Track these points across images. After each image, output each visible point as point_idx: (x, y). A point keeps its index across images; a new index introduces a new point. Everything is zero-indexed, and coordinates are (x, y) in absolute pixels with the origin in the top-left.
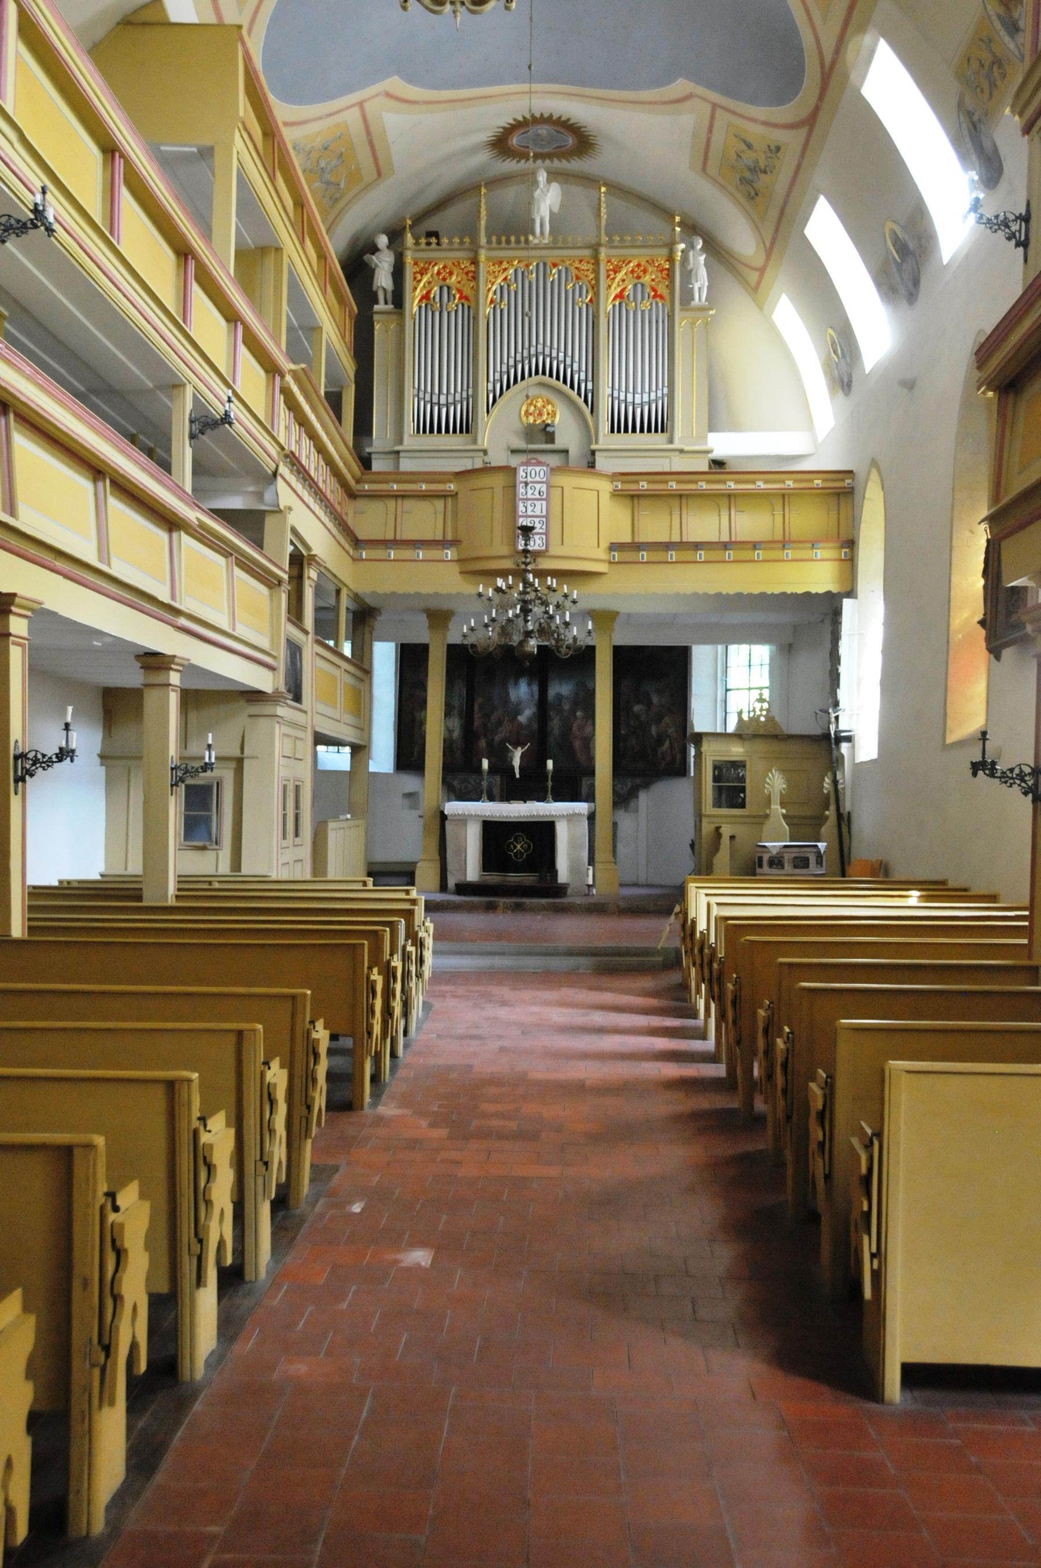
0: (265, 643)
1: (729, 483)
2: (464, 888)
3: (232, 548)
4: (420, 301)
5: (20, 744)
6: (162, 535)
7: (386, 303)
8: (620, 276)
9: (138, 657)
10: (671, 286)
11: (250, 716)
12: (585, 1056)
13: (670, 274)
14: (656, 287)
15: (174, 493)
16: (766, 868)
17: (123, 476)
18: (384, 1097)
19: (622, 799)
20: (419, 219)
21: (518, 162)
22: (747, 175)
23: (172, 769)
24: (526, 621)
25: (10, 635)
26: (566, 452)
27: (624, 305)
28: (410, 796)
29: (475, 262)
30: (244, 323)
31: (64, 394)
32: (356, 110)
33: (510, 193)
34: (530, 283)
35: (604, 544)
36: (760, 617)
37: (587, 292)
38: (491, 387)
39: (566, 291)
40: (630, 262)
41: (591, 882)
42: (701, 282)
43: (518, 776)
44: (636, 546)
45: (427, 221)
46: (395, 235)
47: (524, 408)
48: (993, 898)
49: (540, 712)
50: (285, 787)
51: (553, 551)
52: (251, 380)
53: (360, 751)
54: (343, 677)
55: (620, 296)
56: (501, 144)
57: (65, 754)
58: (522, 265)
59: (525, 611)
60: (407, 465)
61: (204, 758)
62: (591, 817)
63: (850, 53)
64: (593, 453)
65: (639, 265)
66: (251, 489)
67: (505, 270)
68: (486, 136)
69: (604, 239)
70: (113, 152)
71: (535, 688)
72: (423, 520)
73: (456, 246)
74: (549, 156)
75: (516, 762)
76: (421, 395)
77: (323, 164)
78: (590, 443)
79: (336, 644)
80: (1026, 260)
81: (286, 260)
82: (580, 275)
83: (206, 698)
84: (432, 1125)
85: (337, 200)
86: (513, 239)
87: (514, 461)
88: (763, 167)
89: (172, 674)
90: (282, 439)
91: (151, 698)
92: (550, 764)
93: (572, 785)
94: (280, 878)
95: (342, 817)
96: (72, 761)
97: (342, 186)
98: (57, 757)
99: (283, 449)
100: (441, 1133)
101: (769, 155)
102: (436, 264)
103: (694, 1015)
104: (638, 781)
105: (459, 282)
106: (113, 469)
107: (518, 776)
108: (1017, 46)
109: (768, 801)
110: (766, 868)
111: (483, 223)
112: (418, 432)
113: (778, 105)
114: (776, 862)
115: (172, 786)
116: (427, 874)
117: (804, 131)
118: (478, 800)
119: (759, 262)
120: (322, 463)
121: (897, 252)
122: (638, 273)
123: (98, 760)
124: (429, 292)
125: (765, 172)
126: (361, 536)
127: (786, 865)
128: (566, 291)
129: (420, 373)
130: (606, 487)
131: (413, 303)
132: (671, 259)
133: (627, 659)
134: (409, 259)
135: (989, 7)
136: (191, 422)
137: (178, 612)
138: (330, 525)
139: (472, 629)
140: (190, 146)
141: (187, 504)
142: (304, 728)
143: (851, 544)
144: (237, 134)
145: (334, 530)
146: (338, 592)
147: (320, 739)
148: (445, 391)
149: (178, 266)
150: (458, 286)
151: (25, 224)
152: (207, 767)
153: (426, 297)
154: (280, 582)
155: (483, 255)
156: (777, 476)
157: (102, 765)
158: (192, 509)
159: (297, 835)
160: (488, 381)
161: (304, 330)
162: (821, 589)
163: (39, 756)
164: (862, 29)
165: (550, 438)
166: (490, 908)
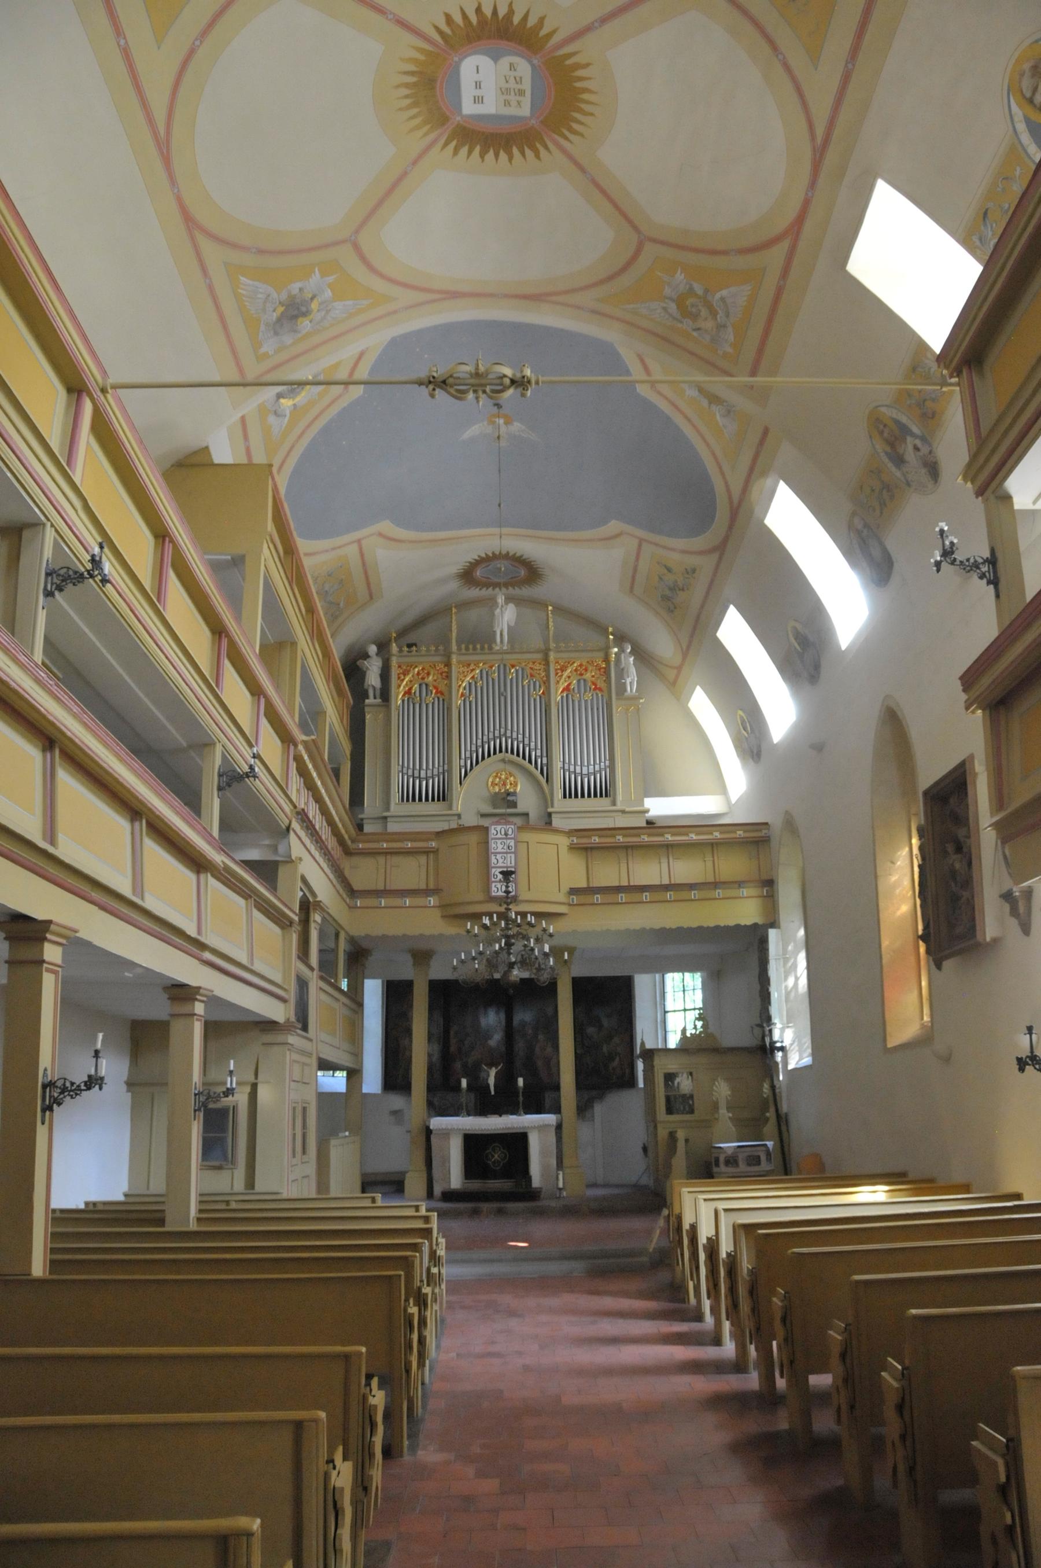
0: (278, 978)
1: (667, 836)
2: (449, 1196)
3: (251, 891)
4: (404, 695)
5: (49, 1072)
6: (190, 876)
8: (566, 674)
9: (166, 989)
10: (608, 680)
11: (264, 1044)
12: (609, 1372)
13: (607, 672)
15: (203, 838)
16: (723, 1168)
17: (158, 817)
18: (421, 1437)
19: (583, 1109)
20: (402, 633)
23: (195, 1095)
24: (509, 954)
25: (44, 961)
26: (527, 815)
28: (396, 1113)
29: (448, 664)
30: (266, 697)
31: (108, 735)
32: (355, 546)
33: (474, 615)
35: (565, 888)
36: (688, 949)
38: (463, 763)
39: (523, 687)
41: (561, 1185)
42: (631, 680)
43: (493, 1093)
44: (590, 890)
45: (409, 633)
46: (383, 647)
47: (491, 780)
48: (966, 1188)
49: (504, 1038)
50: (294, 1108)
52: (269, 745)
53: (354, 1074)
54: (340, 1008)
55: (567, 689)
56: (467, 576)
57: (93, 1082)
58: (486, 666)
59: (509, 945)
60: (393, 827)
61: (226, 1083)
62: (559, 1127)
63: (755, 493)
64: (550, 815)
65: (581, 665)
66: (267, 842)
67: (472, 670)
68: (455, 569)
69: (552, 645)
70: (164, 537)
71: (502, 1016)
72: (409, 873)
73: (433, 652)
74: (506, 585)
75: (492, 1081)
76: (405, 771)
77: (326, 588)
78: (547, 807)
79: (336, 981)
80: (998, 596)
81: (299, 653)
82: (534, 673)
83: (229, 1029)
84: (481, 1474)
85: (336, 617)
86: (478, 646)
87: (485, 822)
88: (681, 586)
89: (197, 1004)
90: (294, 799)
91: (177, 1028)
92: (521, 1082)
93: (537, 1100)
94: (290, 1196)
95: (341, 1135)
96: (101, 1089)
97: (342, 605)
98: (86, 1085)
99: (295, 807)
100: (491, 1485)
103: (699, 1318)
104: (594, 1093)
106: (150, 810)
107: (493, 1093)
108: (904, 475)
109: (715, 1107)
110: (723, 1168)
111: (454, 634)
113: (696, 536)
114: (732, 1161)
115: (195, 1111)
116: (415, 1184)
117: (715, 557)
118: (457, 1115)
119: (677, 660)
120: (325, 823)
121: (799, 644)
122: (580, 672)
123: (124, 1087)
124: (410, 689)
125: (683, 590)
126: (356, 886)
127: (740, 1163)
128: (523, 687)
129: (405, 754)
130: (564, 842)
131: (398, 697)
132: (607, 660)
133: (583, 987)
134: (394, 662)
135: (877, 447)
136: (220, 775)
137: (203, 947)
138: (331, 876)
139: (463, 962)
140: (226, 555)
141: (214, 848)
142: (309, 1055)
143: (769, 883)
144: (265, 546)
145: (334, 881)
146: (337, 935)
147: (325, 1065)
148: (424, 767)
149: (213, 643)
151: (82, 574)
152: (229, 1092)
153: (408, 692)
154: (292, 923)
155: (454, 659)
156: (705, 829)
157: (128, 1091)
158: (219, 853)
159: (304, 1152)
161: (312, 716)
162: (747, 921)
163: (68, 1084)
164: (764, 474)
165: (514, 805)
166: (475, 1213)
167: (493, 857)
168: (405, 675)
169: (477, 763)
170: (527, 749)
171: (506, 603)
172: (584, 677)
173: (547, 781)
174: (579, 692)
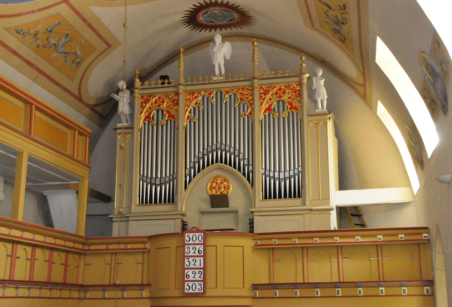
7: (127, 122)
8: (268, 96)
13: (299, 94)
14: (291, 102)
21: (210, 31)
22: (335, 26)
27: (271, 115)
33: (199, 53)
34: (212, 104)
35: (248, 285)
37: (248, 108)
38: (188, 172)
39: (235, 108)
40: (274, 87)
51: (209, 292)
55: (268, 109)
65: (280, 89)
67: (196, 97)
68: (180, 16)
74: (221, 27)
82: (243, 97)
97: (79, 53)
101: (342, 11)
102: (154, 96)
105: (168, 107)
112: (142, 203)
119: (361, 81)
121: (430, 74)
122: (280, 94)
150: (168, 109)
153: (148, 117)
160: (186, 168)
167: (186, 260)
168: (146, 103)
169: (199, 171)
170: (237, 159)
171: (223, 41)
172: (283, 98)
173: (252, 186)
174: (278, 111)
